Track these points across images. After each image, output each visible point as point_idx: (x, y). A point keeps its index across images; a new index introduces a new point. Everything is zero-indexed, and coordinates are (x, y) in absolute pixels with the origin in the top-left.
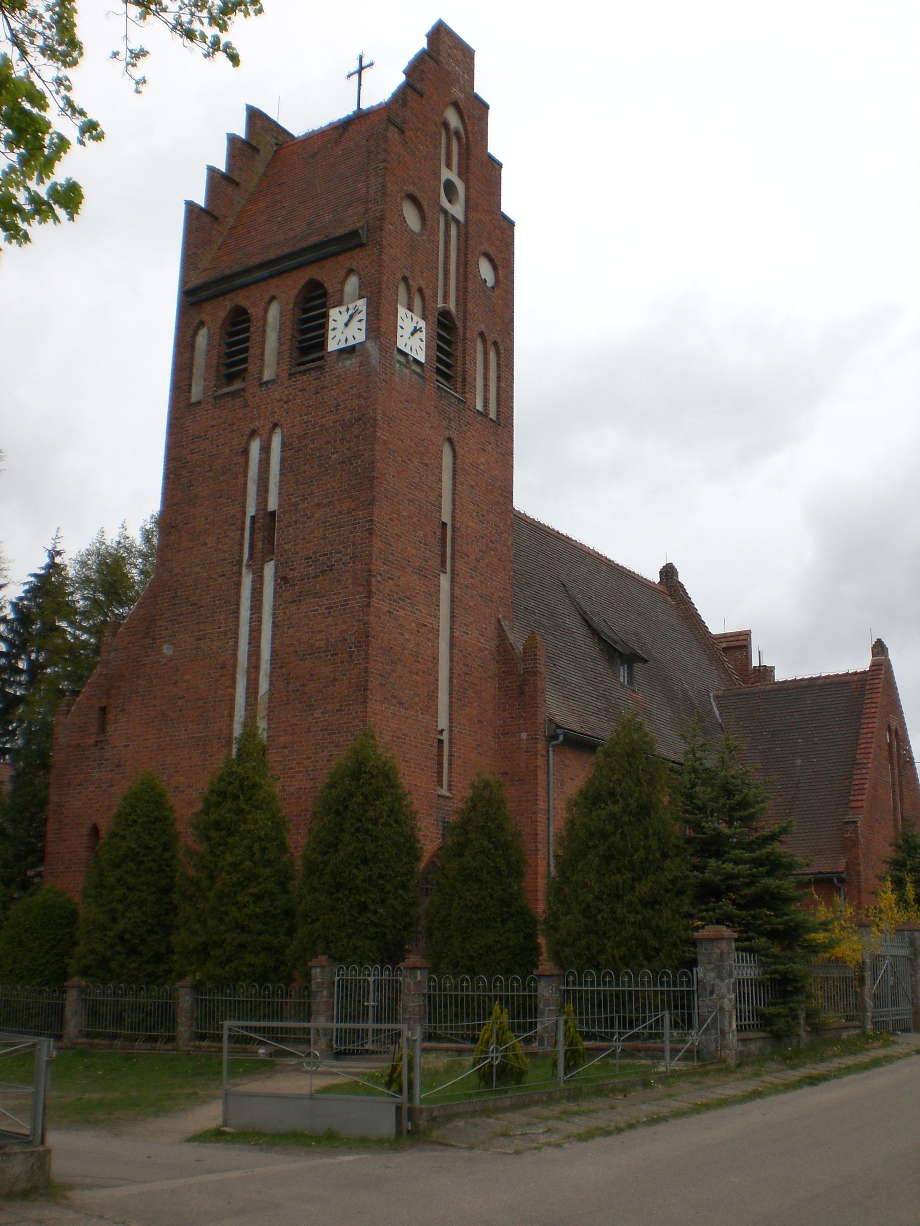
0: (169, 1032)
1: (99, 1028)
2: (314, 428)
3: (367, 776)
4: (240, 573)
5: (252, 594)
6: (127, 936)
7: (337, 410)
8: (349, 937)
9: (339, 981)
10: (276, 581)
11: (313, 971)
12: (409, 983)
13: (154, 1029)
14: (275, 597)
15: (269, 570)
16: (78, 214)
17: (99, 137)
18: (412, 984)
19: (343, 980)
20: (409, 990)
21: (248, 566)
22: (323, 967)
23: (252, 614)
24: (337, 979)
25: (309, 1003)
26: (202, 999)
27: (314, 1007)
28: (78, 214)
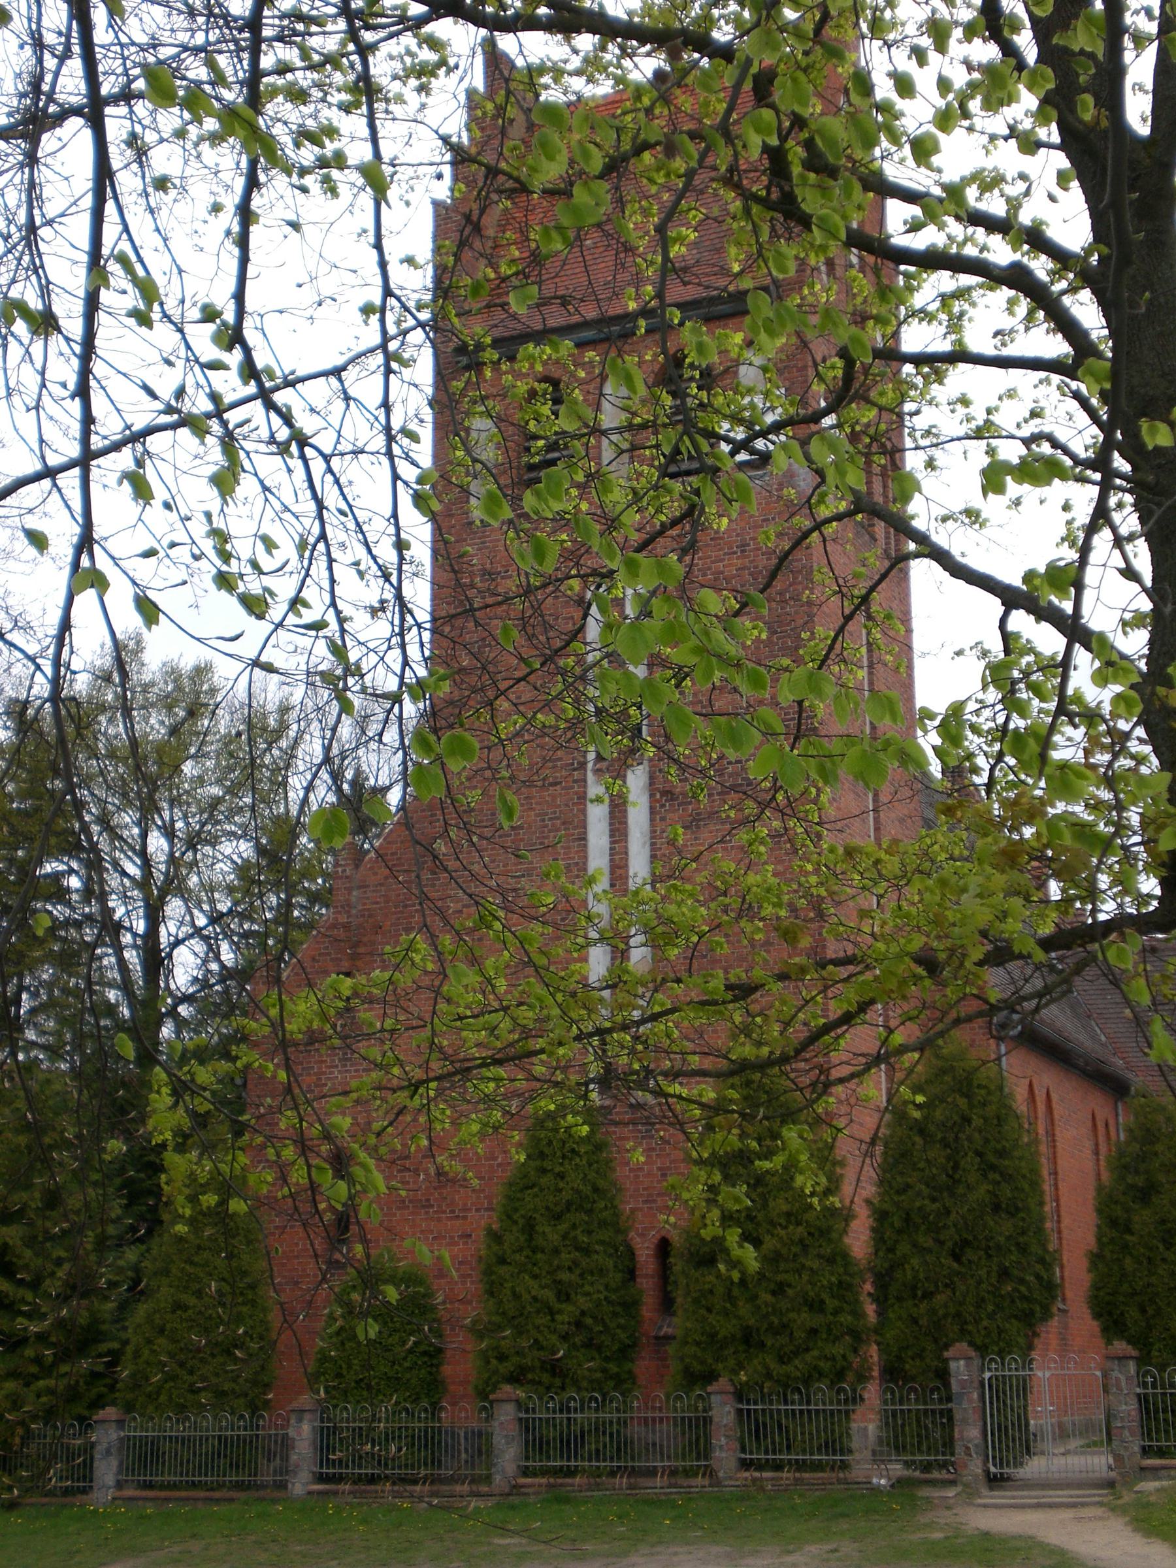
0: (684, 1459)
1: (555, 1460)
2: (704, 575)
3: (983, 1092)
4: (585, 781)
5: (626, 817)
6: (589, 1321)
7: (743, 551)
8: (991, 1316)
9: (990, 1379)
10: (652, 796)
11: (953, 1365)
12: (1117, 1379)
13: (647, 1454)
14: (652, 820)
15: (636, 781)
16: (912, 517)
17: (1067, 501)
18: (1123, 1378)
19: (997, 1378)
20: (1119, 1388)
21: (597, 772)
22: (969, 1358)
23: (612, 843)
24: (987, 1375)
25: (950, 1410)
26: (749, 1410)
27: (957, 1416)
28: (912, 517)
